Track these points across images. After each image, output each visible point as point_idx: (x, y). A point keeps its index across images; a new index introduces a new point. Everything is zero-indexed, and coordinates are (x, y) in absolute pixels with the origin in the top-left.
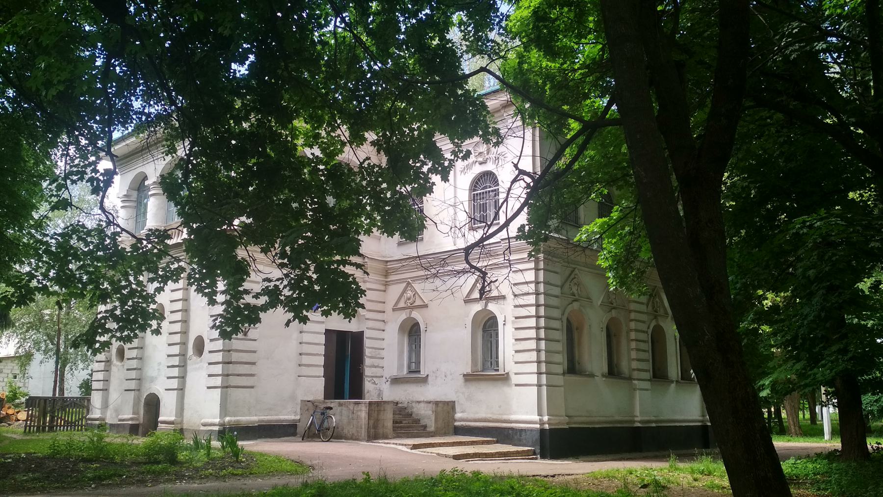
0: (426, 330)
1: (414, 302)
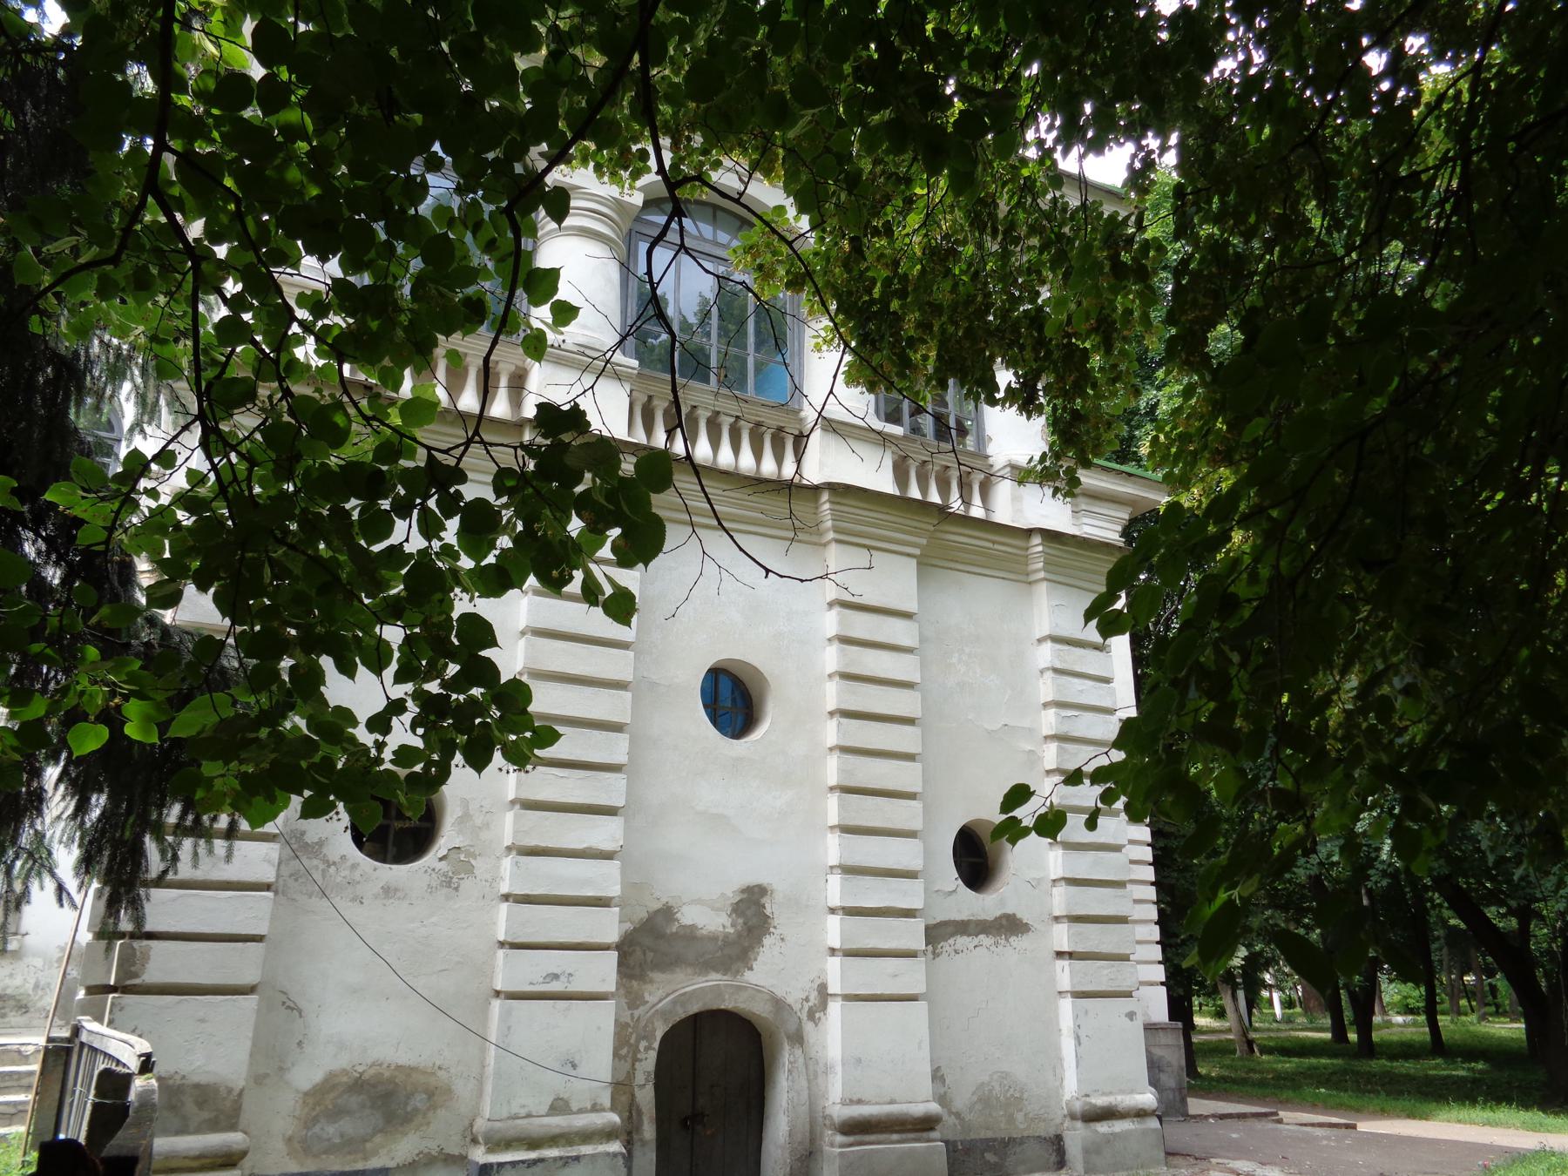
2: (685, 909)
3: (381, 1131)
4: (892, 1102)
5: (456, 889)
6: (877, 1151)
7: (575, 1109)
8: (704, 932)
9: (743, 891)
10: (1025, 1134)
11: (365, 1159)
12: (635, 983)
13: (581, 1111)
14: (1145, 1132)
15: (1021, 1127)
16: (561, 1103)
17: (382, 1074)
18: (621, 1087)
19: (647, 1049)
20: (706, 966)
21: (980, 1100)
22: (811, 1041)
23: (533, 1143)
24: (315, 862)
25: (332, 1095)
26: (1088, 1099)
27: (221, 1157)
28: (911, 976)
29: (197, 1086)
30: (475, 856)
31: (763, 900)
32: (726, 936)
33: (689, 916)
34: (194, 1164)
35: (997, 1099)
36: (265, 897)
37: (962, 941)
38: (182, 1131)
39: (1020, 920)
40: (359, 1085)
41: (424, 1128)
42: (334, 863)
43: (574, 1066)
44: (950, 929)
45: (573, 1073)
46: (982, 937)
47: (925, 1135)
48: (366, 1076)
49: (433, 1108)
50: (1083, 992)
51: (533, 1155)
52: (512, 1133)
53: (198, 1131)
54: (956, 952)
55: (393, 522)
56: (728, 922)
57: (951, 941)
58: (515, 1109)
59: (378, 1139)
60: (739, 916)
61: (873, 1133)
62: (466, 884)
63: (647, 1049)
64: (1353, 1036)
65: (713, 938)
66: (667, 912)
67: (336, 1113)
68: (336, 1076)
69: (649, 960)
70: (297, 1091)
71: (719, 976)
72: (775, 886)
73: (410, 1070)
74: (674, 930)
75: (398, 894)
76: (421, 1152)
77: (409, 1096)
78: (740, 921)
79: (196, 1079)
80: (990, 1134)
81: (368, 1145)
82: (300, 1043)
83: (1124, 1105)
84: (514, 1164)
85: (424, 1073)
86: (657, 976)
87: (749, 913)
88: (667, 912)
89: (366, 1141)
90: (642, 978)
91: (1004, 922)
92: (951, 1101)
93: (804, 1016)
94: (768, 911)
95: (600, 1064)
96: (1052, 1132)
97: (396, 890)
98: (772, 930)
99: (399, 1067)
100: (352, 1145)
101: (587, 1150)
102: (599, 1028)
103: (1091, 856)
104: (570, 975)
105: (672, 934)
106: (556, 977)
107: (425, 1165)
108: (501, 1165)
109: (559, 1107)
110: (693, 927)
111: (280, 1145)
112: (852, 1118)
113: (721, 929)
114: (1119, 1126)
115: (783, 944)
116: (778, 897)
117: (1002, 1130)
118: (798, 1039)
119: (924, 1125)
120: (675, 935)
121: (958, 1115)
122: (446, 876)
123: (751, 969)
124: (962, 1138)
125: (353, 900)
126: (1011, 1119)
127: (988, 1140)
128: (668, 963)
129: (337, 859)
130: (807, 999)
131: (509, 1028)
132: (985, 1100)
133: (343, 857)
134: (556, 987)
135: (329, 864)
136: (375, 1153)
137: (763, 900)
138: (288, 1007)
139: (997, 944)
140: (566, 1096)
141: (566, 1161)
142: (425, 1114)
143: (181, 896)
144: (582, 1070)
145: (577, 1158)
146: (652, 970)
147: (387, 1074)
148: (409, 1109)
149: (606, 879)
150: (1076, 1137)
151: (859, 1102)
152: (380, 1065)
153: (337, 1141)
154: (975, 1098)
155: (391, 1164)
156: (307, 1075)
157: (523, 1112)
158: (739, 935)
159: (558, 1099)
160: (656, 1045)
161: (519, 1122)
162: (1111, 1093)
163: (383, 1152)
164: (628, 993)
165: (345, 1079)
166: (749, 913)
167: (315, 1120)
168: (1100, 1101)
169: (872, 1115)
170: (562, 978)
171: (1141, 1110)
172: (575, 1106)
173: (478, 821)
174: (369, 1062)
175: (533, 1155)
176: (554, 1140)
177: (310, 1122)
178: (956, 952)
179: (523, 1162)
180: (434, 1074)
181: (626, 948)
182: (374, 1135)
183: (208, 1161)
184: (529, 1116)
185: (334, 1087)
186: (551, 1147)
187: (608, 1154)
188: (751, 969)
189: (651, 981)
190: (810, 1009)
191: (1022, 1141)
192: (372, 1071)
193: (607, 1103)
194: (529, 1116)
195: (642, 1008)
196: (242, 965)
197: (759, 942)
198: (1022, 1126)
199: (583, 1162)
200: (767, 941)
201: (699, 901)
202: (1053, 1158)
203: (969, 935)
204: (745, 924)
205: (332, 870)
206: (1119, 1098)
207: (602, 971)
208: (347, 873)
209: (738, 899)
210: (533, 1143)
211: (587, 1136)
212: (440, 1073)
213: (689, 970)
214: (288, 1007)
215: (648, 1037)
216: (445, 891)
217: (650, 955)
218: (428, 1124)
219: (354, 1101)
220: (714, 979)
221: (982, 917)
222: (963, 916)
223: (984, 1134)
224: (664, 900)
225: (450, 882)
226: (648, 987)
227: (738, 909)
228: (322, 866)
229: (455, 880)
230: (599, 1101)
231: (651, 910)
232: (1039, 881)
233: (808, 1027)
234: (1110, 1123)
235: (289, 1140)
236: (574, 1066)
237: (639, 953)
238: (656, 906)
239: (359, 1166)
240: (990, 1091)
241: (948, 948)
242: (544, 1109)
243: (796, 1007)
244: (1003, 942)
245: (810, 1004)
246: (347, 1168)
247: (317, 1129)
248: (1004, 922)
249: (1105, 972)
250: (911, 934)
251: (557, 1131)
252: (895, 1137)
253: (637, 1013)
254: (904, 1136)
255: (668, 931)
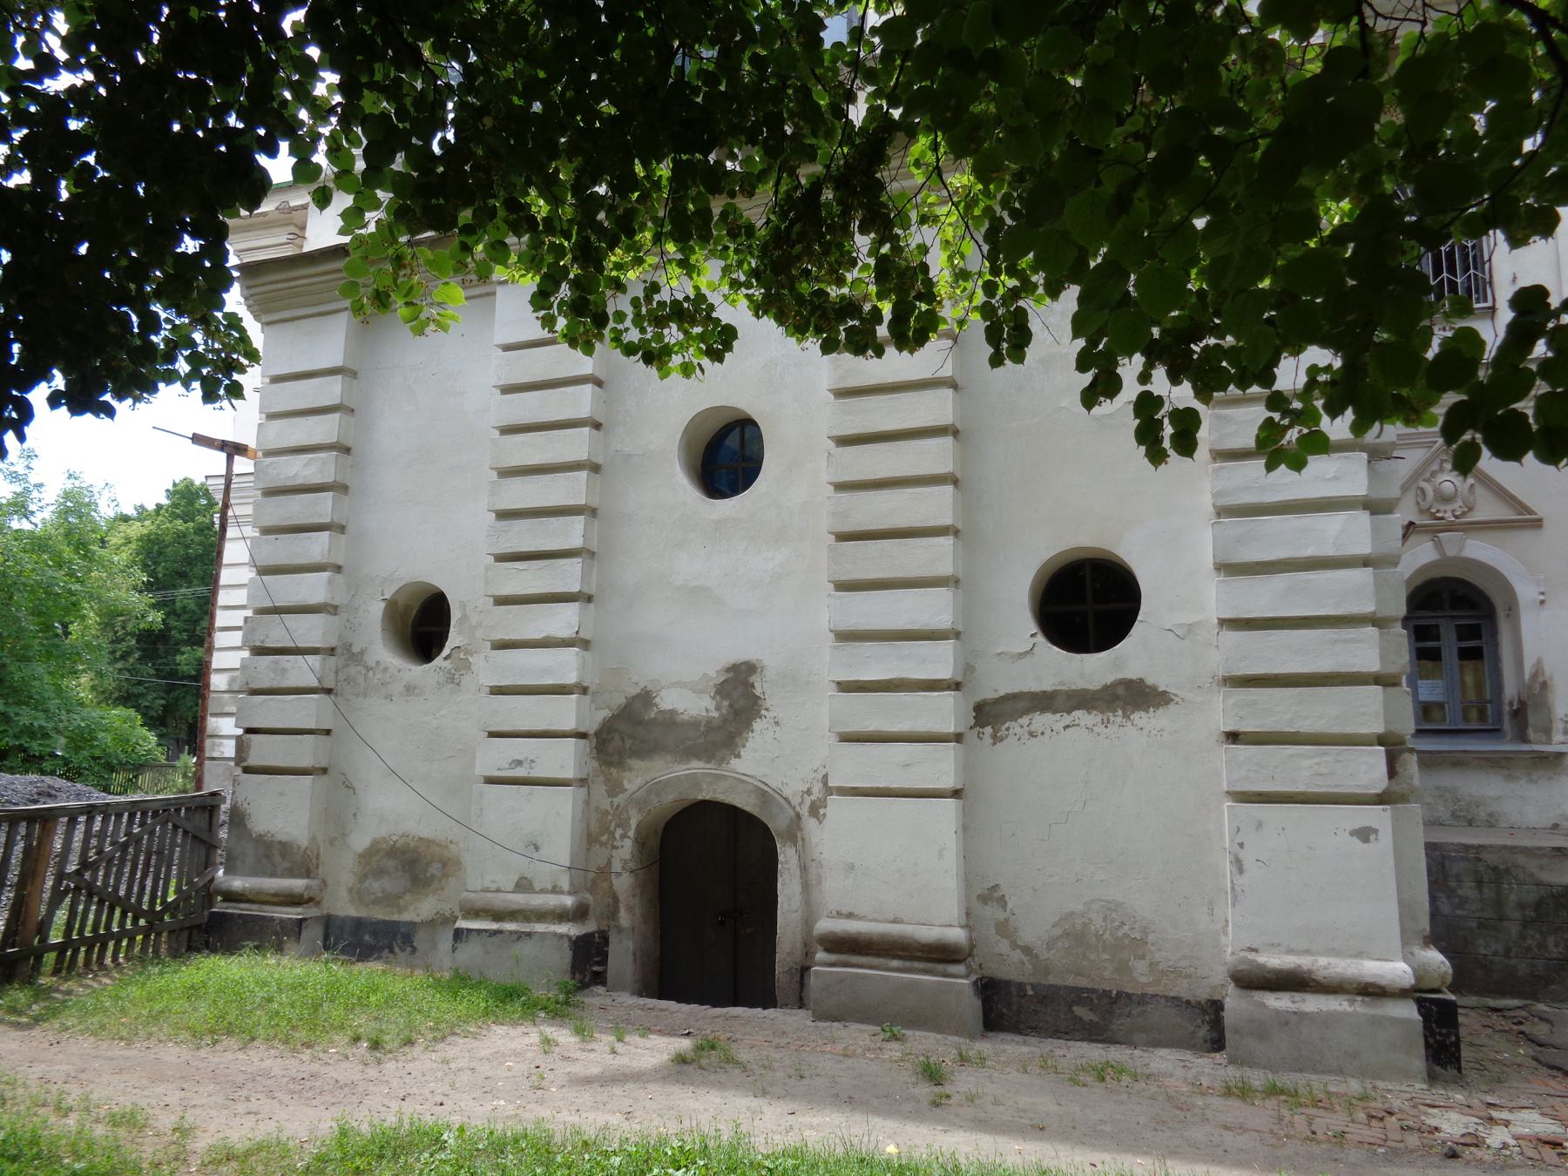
0: (1542, 602)
1: (1471, 509)
2: (664, 693)
3: (409, 891)
4: (895, 921)
5: (458, 684)
6: (865, 976)
7: (537, 889)
8: (685, 717)
9: (728, 670)
10: (1151, 991)
11: (400, 912)
12: (614, 770)
13: (543, 891)
14: (1376, 1022)
15: (1140, 977)
16: (525, 882)
17: (409, 844)
18: (589, 877)
19: (623, 836)
20: (690, 753)
21: (1066, 934)
22: (814, 840)
23: (498, 916)
24: (359, 668)
25: (376, 858)
26: (1251, 956)
27: (287, 896)
28: (940, 767)
29: (280, 843)
30: (470, 653)
31: (752, 679)
32: (710, 721)
33: (670, 700)
34: (275, 899)
35: (1099, 937)
36: (313, 699)
37: (1041, 720)
38: (273, 875)
39: (1154, 689)
40: (393, 851)
41: (439, 892)
42: (372, 669)
43: (537, 848)
44: (1022, 705)
45: (535, 855)
46: (1078, 714)
47: (940, 967)
48: (398, 845)
49: (446, 876)
50: (1260, 794)
51: (495, 926)
52: (479, 904)
53: (282, 876)
54: (1032, 734)
55: (27, 399)
56: (711, 705)
57: (1024, 720)
58: (488, 884)
59: (408, 897)
60: (723, 698)
61: (867, 954)
62: (466, 680)
63: (623, 836)
64: (133, 900)
65: (694, 724)
66: (646, 698)
67: (380, 873)
68: (378, 843)
69: (627, 746)
70: (355, 853)
71: (701, 764)
72: (766, 662)
73: (429, 842)
74: (653, 716)
75: (416, 691)
76: (438, 913)
77: (429, 864)
78: (726, 703)
79: (279, 837)
80: (1083, 983)
81: (401, 901)
82: (355, 815)
83: (1326, 973)
84: (479, 931)
85: (440, 845)
86: (635, 763)
87: (735, 694)
88: (646, 698)
89: (401, 897)
90: (620, 764)
91: (1121, 691)
92: (1016, 930)
93: (804, 811)
94: (758, 692)
95: (560, 846)
96: (1202, 994)
97: (415, 688)
98: (763, 712)
99: (421, 839)
100: (391, 900)
101: (540, 928)
102: (558, 813)
103: (1280, 581)
104: (532, 761)
105: (651, 720)
106: (519, 763)
107: (441, 923)
108: (469, 931)
109: (523, 885)
110: (673, 712)
111: (344, 893)
112: (833, 933)
113: (704, 713)
114: (1312, 1003)
115: (776, 728)
116: (770, 674)
117: (1105, 977)
118: (794, 833)
119: (940, 955)
120: (654, 721)
121: (1027, 950)
122: (450, 674)
123: (738, 756)
124: (1032, 980)
125: (386, 698)
126: (1123, 968)
127: (1082, 990)
128: (647, 750)
129: (374, 665)
130: (809, 792)
131: (481, 810)
132: (1076, 936)
133: (378, 663)
134: (520, 772)
135: (368, 669)
136: (406, 909)
137: (752, 679)
138: (347, 786)
139: (1106, 725)
140: (529, 876)
141: (520, 936)
142: (440, 881)
143: (265, 701)
144: (544, 853)
145: (529, 935)
146: (630, 757)
147: (412, 844)
148: (428, 875)
149: (564, 666)
150: (1235, 1004)
151: (850, 916)
152: (408, 836)
153: (380, 895)
154: (1058, 931)
155: (417, 920)
156: (360, 841)
157: (493, 887)
158: (725, 720)
159: (522, 878)
160: (631, 833)
161: (488, 895)
162: (1307, 952)
163: (411, 908)
164: (608, 780)
165: (384, 846)
166: (735, 694)
167: (365, 876)
168: (1276, 961)
169: (860, 933)
170: (525, 764)
171: (1373, 985)
172: (537, 887)
173: (474, 620)
174: (401, 833)
175: (495, 926)
176: (513, 915)
177: (363, 877)
178: (1032, 734)
179: (486, 931)
180: (446, 847)
181: (604, 736)
182: (404, 893)
183: (283, 899)
184: (498, 890)
185: (378, 851)
186: (511, 921)
187: (555, 934)
188: (738, 756)
189: (630, 769)
190: (813, 803)
191: (1143, 999)
192: (402, 841)
193: (566, 886)
194: (498, 890)
195: (621, 796)
196: (302, 752)
197: (748, 726)
198: (1144, 980)
199: (535, 938)
200: (758, 725)
201: (679, 684)
202: (1203, 1032)
203: (1055, 712)
204: (731, 706)
205: (371, 672)
206: (1323, 961)
207: (563, 758)
208: (379, 676)
209: (722, 679)
210: (498, 916)
211: (541, 915)
212: (452, 847)
213: (669, 758)
214: (347, 786)
215: (623, 824)
216: (450, 686)
217: (629, 742)
218: (443, 889)
219: (390, 864)
220: (697, 766)
221: (1080, 684)
222: (1047, 685)
223: (1071, 981)
224: (642, 685)
225: (453, 679)
226: (627, 774)
227: (722, 690)
228: (364, 672)
229: (457, 676)
230: (558, 883)
231: (629, 696)
232: (1191, 628)
233: (810, 824)
234: (1297, 996)
235: (350, 890)
236: (537, 848)
237: (617, 737)
238: (634, 691)
239: (395, 918)
240: (1085, 925)
241: (1018, 729)
242: (511, 887)
243: (795, 801)
244: (1119, 720)
245: (813, 798)
246: (387, 919)
247: (366, 884)
248: (1121, 691)
249: (1307, 763)
250: (944, 713)
251: (515, 907)
252: (895, 963)
253: (616, 801)
254: (908, 964)
255: (646, 718)
